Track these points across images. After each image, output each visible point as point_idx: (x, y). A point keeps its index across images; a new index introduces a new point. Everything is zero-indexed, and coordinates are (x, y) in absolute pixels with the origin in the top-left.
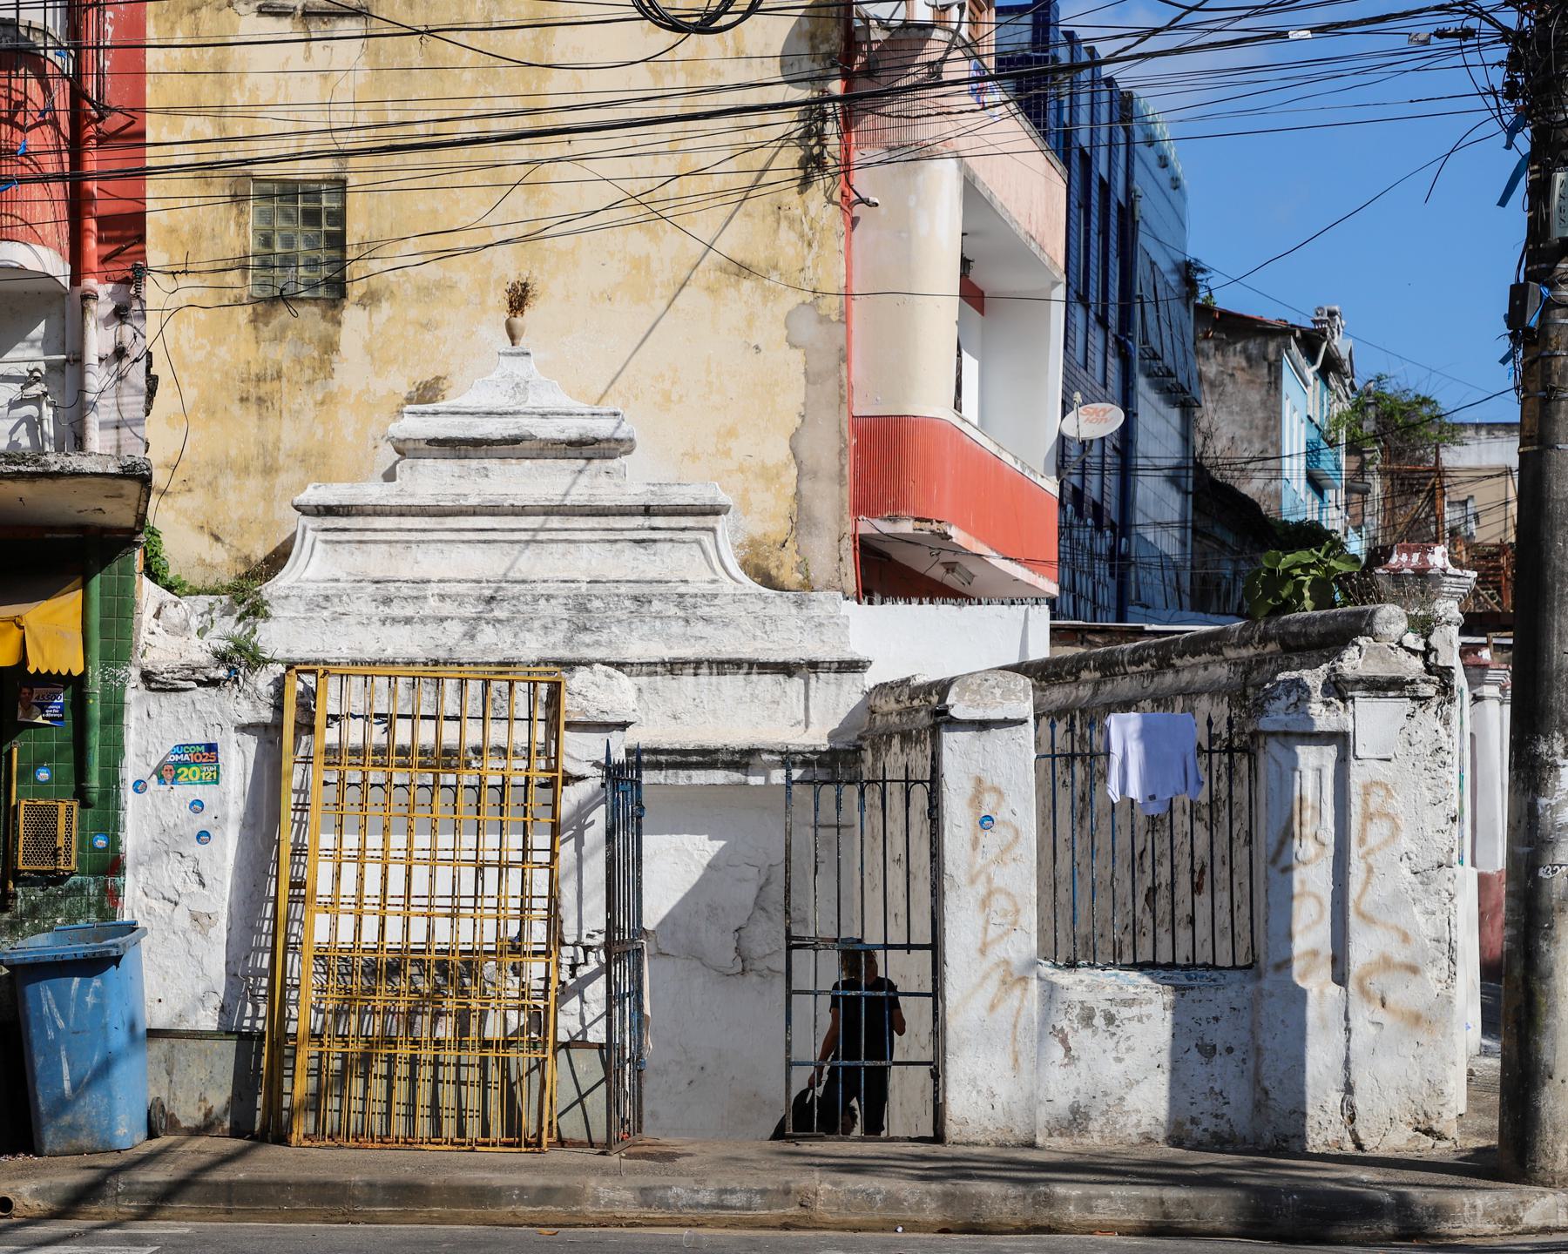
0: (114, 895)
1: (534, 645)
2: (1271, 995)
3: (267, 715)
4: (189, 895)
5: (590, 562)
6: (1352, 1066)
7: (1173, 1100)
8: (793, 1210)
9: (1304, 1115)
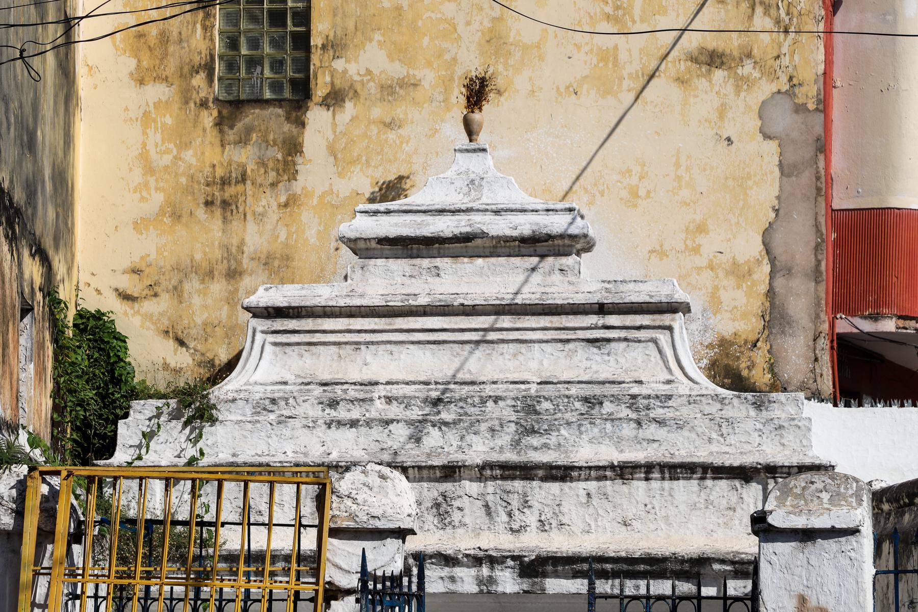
1: (481, 448)
5: (541, 363)
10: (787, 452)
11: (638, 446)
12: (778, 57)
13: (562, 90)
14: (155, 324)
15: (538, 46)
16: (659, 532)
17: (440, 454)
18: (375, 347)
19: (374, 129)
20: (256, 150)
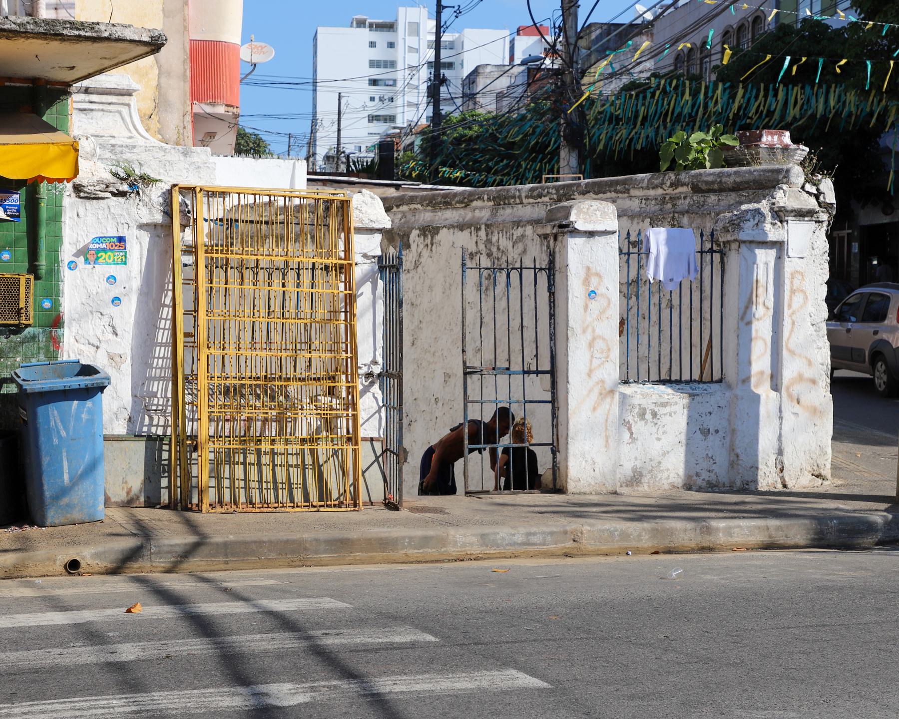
0: (56, 342)
2: (742, 398)
3: (159, 218)
4: (107, 341)
6: (783, 439)
7: (687, 462)
8: (570, 544)
9: (757, 468)
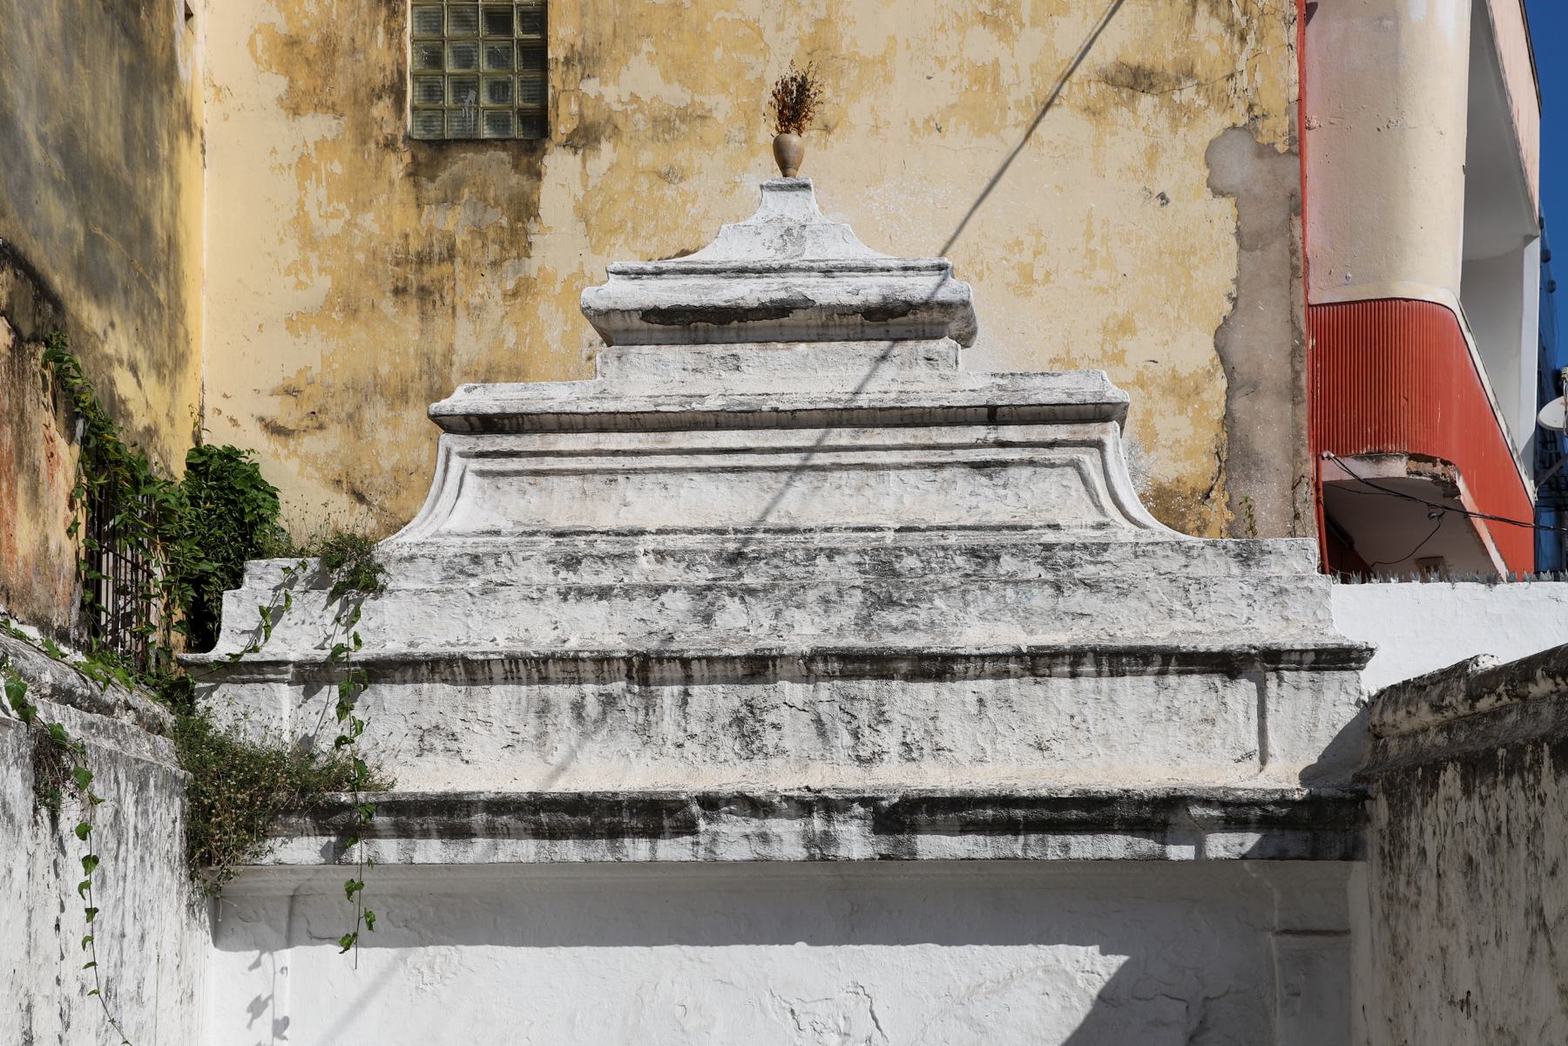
1: (808, 630)
5: (900, 500)
10: (1293, 631)
11: (1058, 624)
12: (1232, 76)
13: (920, 125)
14: (320, 470)
15: (883, 61)
16: (1095, 760)
17: (742, 640)
18: (639, 477)
19: (644, 183)
20: (469, 213)
